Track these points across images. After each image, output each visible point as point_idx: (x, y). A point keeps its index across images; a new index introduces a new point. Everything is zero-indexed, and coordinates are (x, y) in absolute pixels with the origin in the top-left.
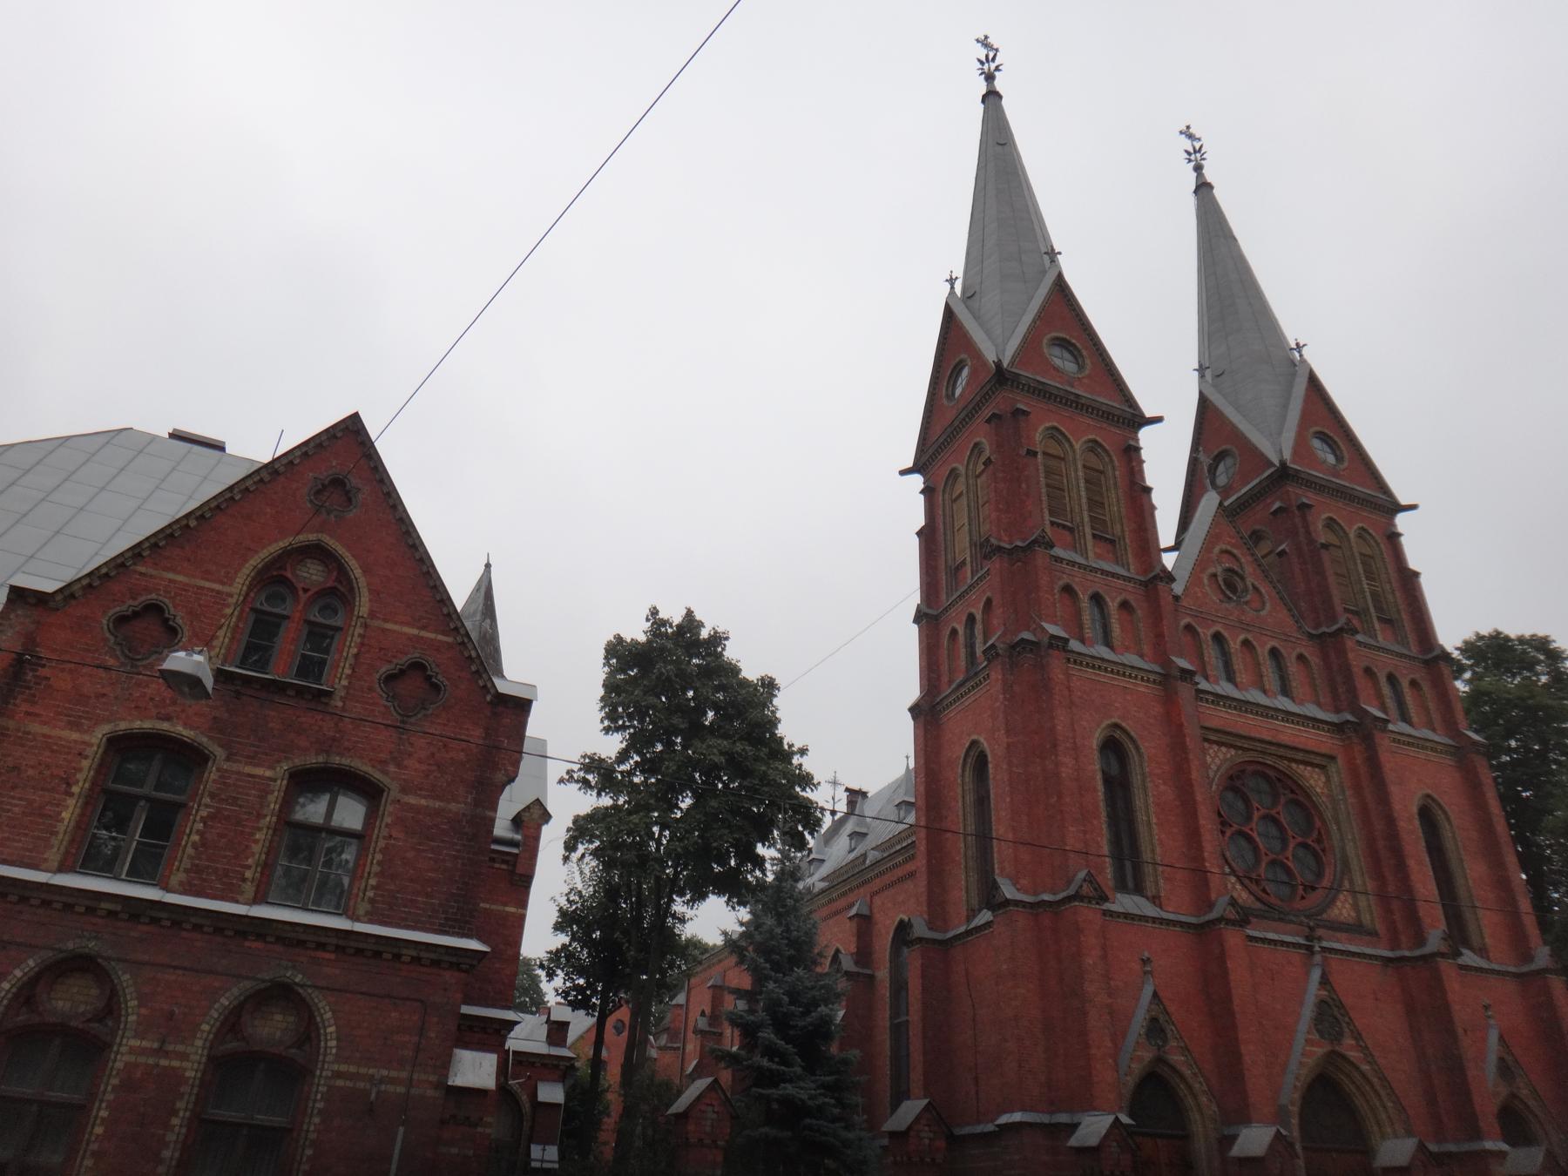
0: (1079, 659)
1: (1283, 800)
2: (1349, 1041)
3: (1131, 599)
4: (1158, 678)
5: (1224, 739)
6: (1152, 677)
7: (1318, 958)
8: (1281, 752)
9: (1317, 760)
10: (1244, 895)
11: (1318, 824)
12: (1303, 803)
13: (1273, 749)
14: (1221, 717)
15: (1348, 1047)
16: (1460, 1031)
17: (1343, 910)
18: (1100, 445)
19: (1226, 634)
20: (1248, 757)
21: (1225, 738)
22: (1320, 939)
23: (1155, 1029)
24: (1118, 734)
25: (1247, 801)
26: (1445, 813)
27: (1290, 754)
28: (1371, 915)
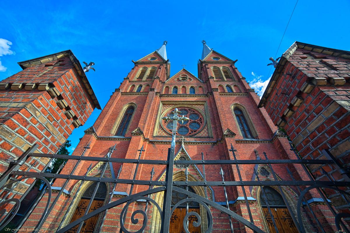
3: (236, 84)
8: (188, 103)
9: (201, 103)
10: (165, 134)
13: (186, 103)
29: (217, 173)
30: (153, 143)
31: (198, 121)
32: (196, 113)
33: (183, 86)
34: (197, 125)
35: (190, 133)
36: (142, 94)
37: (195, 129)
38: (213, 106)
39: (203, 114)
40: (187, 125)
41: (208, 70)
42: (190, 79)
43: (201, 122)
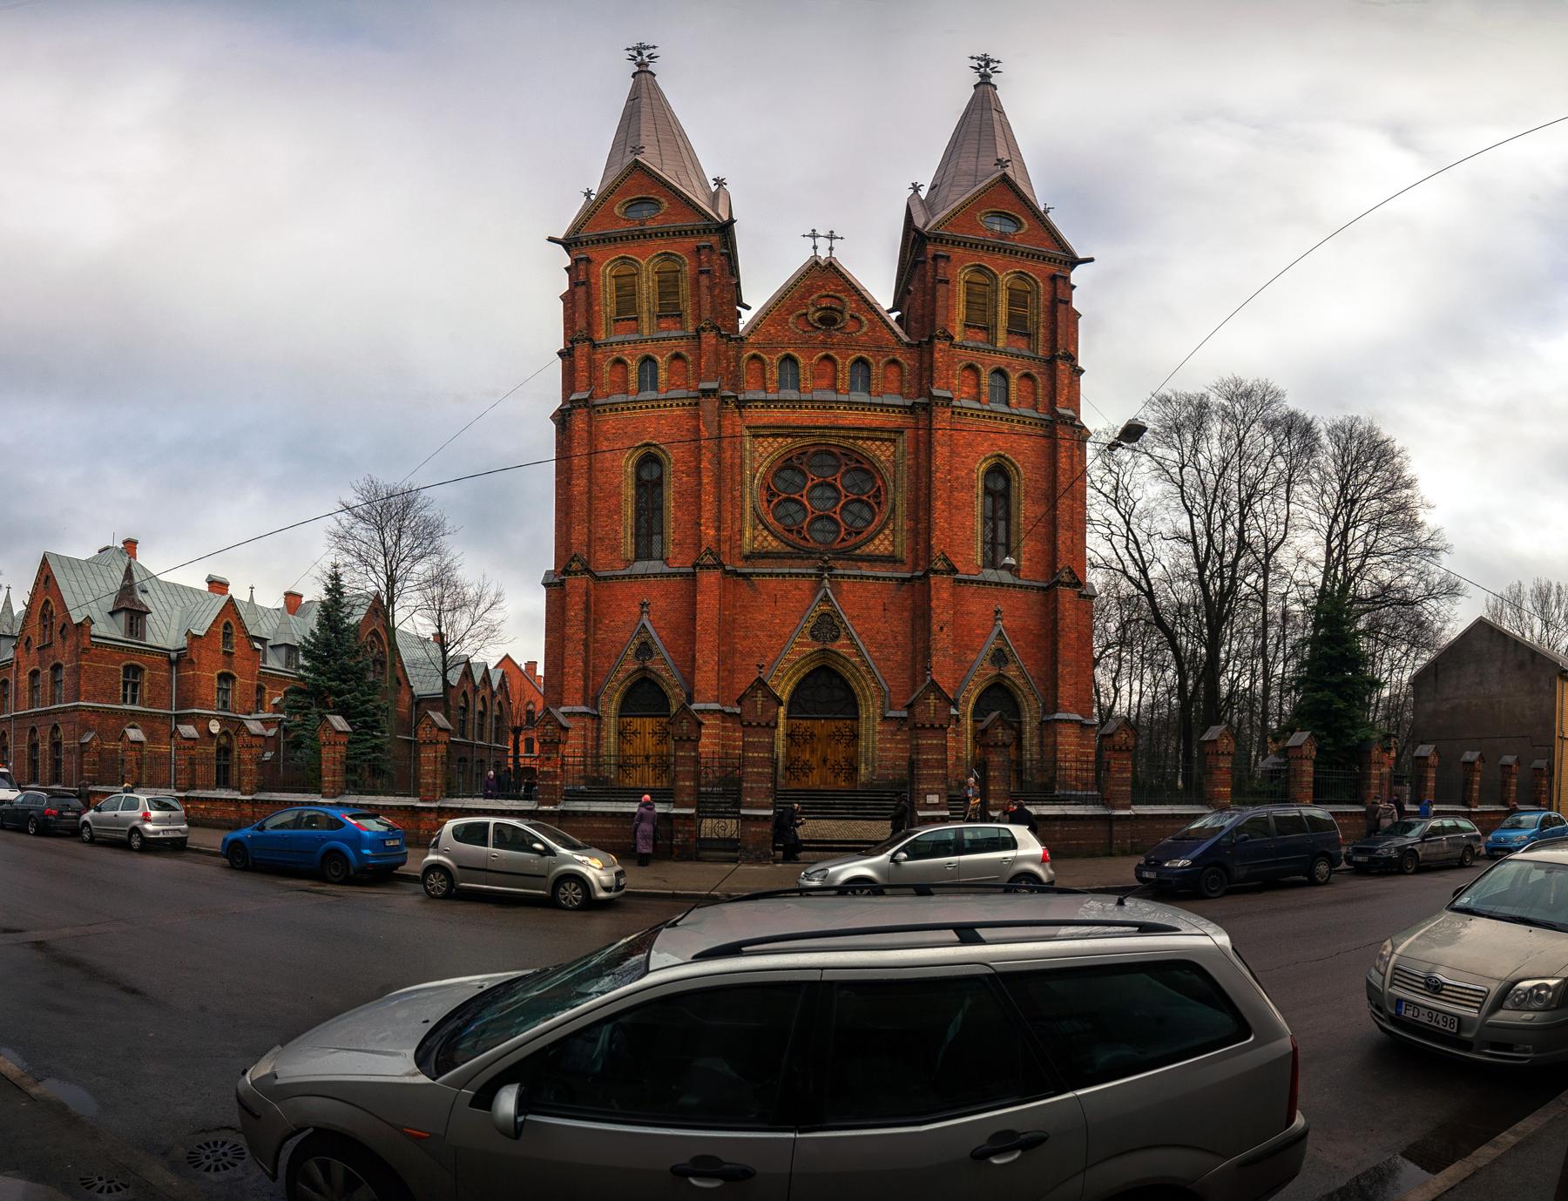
1: (805, 468)
3: (1033, 372)
9: (886, 435)
10: (774, 544)
12: (865, 469)
13: (833, 432)
14: (776, 416)
15: (841, 646)
16: (935, 628)
17: (881, 545)
20: (808, 441)
21: (777, 431)
22: (831, 568)
23: (1000, 657)
24: (653, 450)
25: (804, 475)
28: (902, 552)
34: (866, 513)
37: (859, 524)
38: (922, 456)
39: (888, 477)
41: (941, 288)
43: (879, 504)
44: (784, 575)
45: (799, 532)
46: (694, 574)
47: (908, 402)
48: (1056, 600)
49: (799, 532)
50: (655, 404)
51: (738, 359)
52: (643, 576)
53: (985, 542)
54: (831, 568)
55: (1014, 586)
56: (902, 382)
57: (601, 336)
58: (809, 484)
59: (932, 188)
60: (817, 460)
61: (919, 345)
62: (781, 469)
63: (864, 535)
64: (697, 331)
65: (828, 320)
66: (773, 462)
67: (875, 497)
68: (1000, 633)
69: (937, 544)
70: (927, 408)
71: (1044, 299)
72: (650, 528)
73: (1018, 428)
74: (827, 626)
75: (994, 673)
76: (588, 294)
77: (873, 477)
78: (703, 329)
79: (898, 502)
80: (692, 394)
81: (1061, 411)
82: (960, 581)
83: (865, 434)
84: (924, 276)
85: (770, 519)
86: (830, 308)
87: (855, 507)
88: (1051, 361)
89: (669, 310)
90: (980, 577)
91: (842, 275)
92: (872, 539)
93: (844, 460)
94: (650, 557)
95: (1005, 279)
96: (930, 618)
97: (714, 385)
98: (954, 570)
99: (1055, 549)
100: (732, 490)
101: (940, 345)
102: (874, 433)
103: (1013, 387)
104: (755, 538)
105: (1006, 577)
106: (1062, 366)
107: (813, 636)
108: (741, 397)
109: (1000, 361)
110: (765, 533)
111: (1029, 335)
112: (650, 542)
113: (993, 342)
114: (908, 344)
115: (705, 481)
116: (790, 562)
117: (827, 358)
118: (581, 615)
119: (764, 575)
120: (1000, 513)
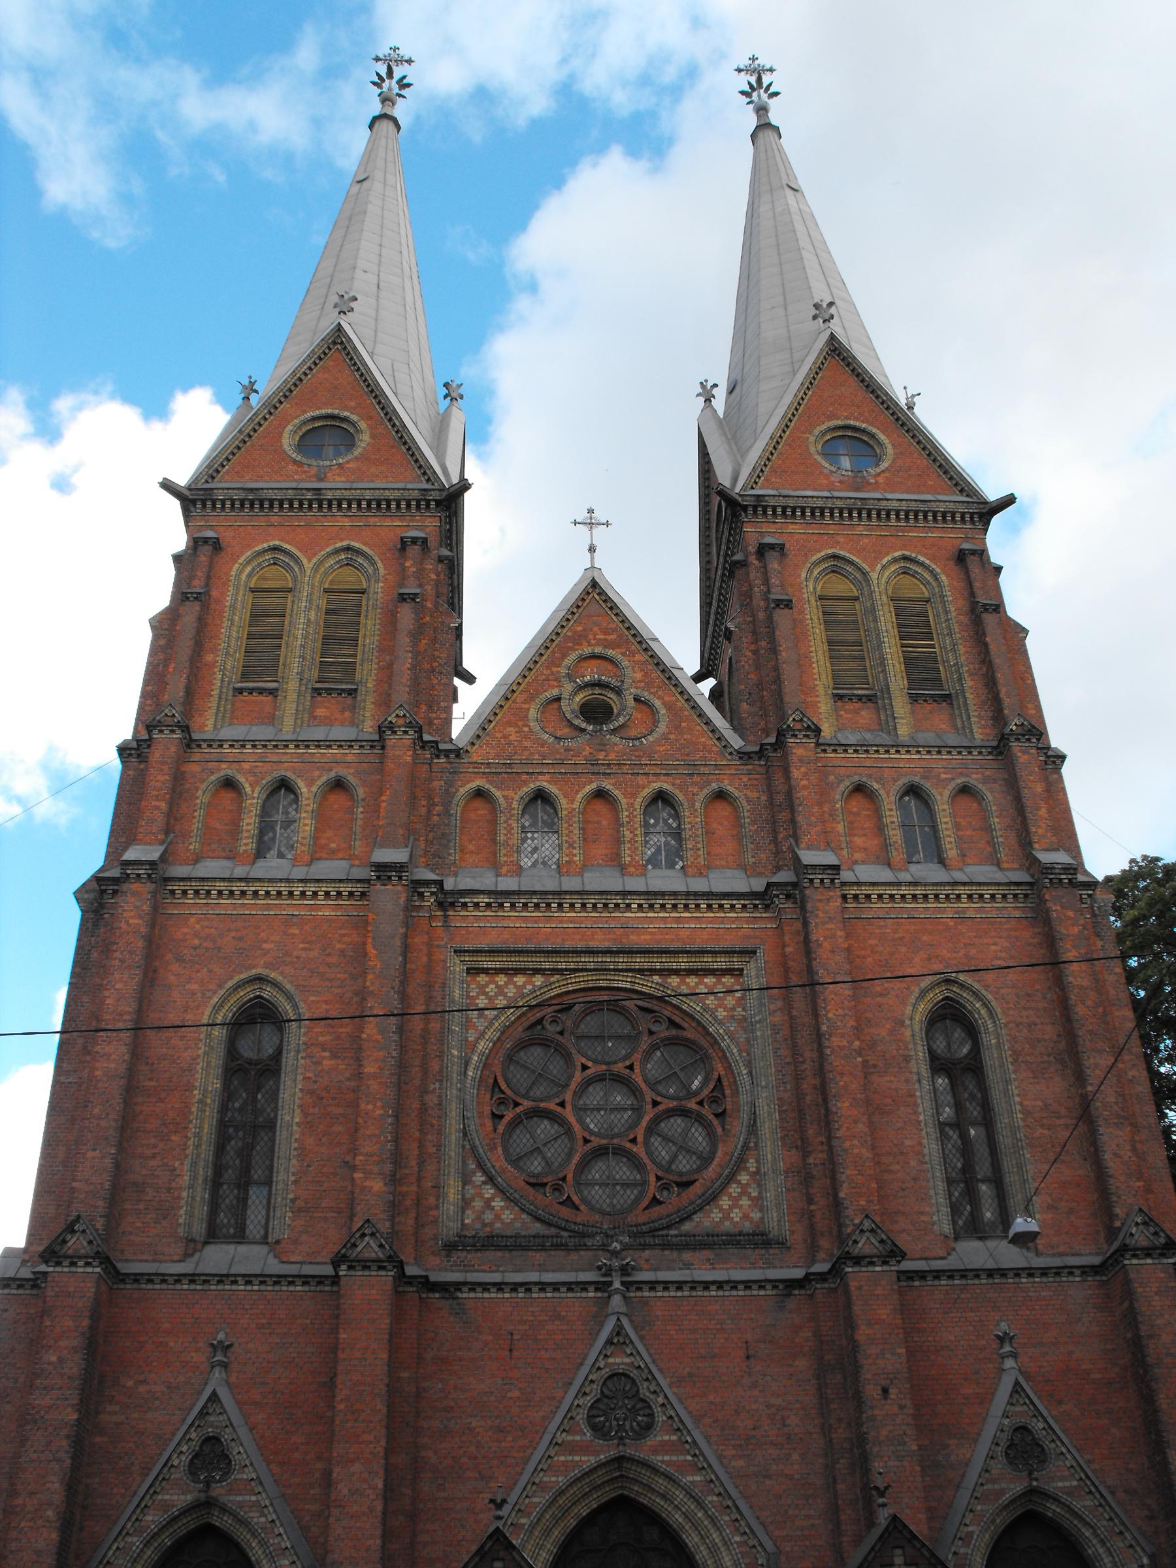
0: (284, 888)
1: (568, 1041)
2: (662, 1436)
3: (974, 780)
4: (358, 888)
5: (513, 962)
6: (345, 889)
7: (617, 1300)
8: (639, 962)
9: (721, 963)
10: (507, 1216)
11: (720, 1068)
12: (685, 1039)
13: (622, 961)
14: (514, 925)
16: (872, 1391)
17: (733, 1211)
18: (358, 552)
19: (553, 789)
20: (574, 982)
21: (516, 958)
23: (1023, 1447)
24: (268, 992)
25: (567, 1058)
26: (986, 1005)
27: (657, 963)
29: (795, 1456)
30: (447, 1290)
31: (701, 1103)
32: (687, 1040)
33: (594, 786)
34: (698, 1136)
35: (655, 1201)
36: (315, 894)
37: (684, 1164)
40: (634, 1141)
41: (782, 618)
42: (645, 703)
43: (720, 1116)
44: (527, 1286)
45: (557, 1188)
46: (335, 1280)
47: (758, 885)
48: (1129, 1294)
49: (557, 1188)
50: (284, 889)
51: (448, 795)
52: (222, 1279)
53: (950, 1182)
54: (625, 1270)
55: (1030, 1272)
56: (739, 838)
57: (207, 725)
58: (578, 1076)
59: (731, 391)
60: (590, 1025)
61: (761, 754)
62: (523, 1045)
63: (697, 1189)
64: (381, 731)
65: (596, 713)
66: (505, 1030)
67: (714, 1100)
68: (1017, 1388)
69: (856, 1202)
70: (794, 892)
71: (954, 606)
72: (246, 1169)
73: (971, 909)
74: (621, 1405)
75: (1016, 1487)
76: (202, 624)
77: (705, 1059)
78: (392, 728)
79: (763, 1110)
80: (358, 873)
81: (1046, 857)
82: (910, 1275)
83: (682, 962)
84: (749, 595)
85: (497, 1160)
86: (599, 684)
87: (677, 1125)
88: (1001, 748)
89: (334, 684)
90: (951, 1263)
91: (613, 607)
92: (715, 1197)
93: (645, 1022)
94: (240, 1236)
95: (881, 576)
96: (857, 1368)
97: (399, 855)
98: (895, 1253)
99: (1101, 1175)
100: (424, 1091)
101: (800, 749)
102: (698, 960)
103: (944, 821)
104: (466, 1203)
105: (1011, 1256)
106: (1022, 754)
107: (594, 1428)
108: (449, 884)
109: (910, 767)
110: (489, 1191)
111: (947, 698)
112: (243, 1201)
113: (888, 724)
114: (743, 756)
115: (370, 1069)
116: (539, 1257)
117: (600, 794)
118: (74, 1366)
119: (485, 1286)
120: (975, 1112)
